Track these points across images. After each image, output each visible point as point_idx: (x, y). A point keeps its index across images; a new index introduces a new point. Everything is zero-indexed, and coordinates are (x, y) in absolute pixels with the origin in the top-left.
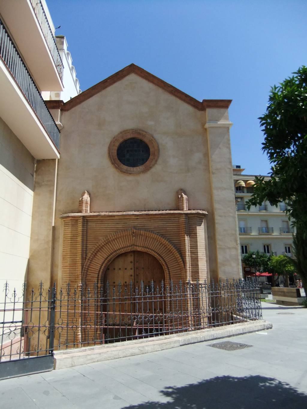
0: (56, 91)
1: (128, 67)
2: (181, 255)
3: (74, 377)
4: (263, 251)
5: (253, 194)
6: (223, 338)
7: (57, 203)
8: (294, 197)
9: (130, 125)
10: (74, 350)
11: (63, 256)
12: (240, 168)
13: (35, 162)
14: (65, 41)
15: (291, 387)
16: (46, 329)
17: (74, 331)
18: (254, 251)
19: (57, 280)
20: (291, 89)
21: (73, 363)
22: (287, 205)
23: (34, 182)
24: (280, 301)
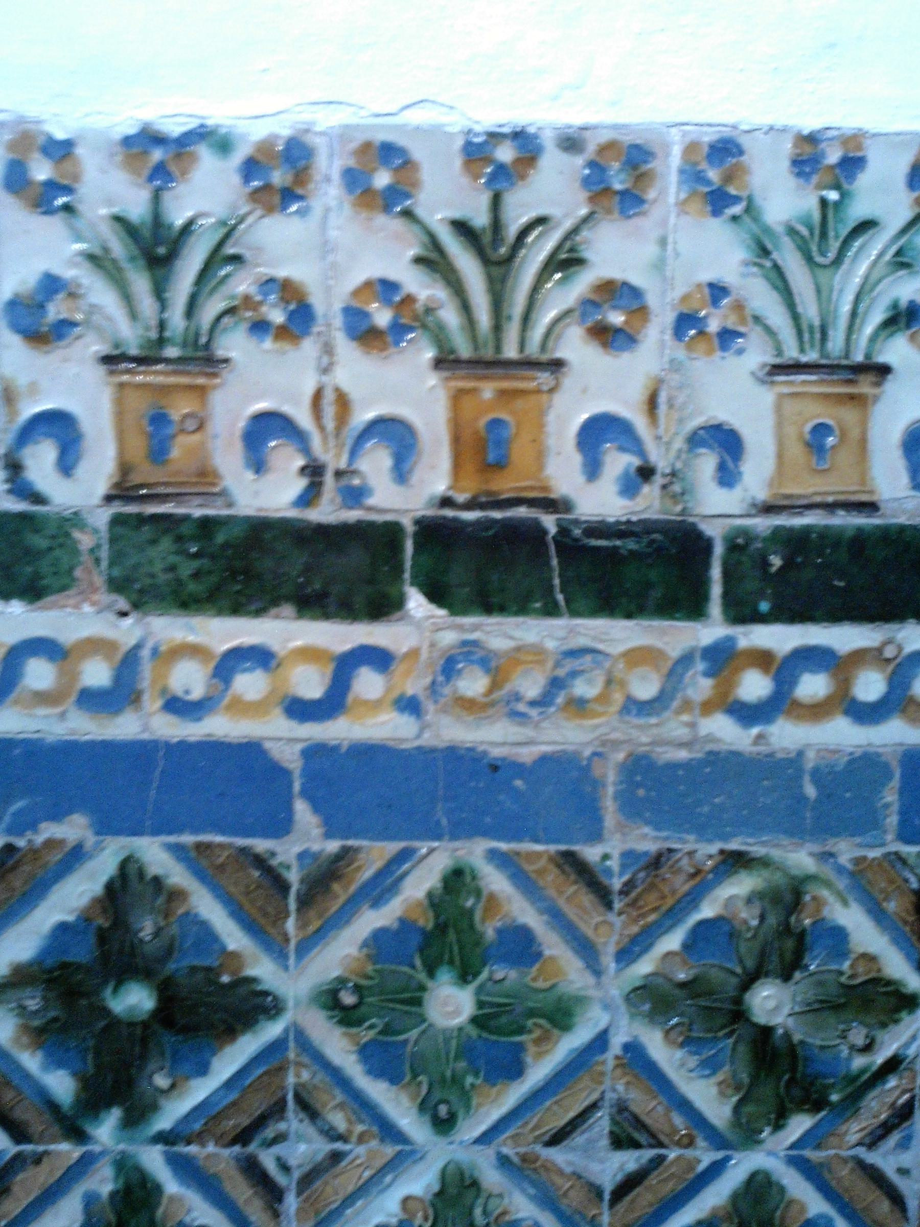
0: (401, 839)
2: (96, 550)
10: (811, 490)
13: (638, 172)
18: (206, 208)
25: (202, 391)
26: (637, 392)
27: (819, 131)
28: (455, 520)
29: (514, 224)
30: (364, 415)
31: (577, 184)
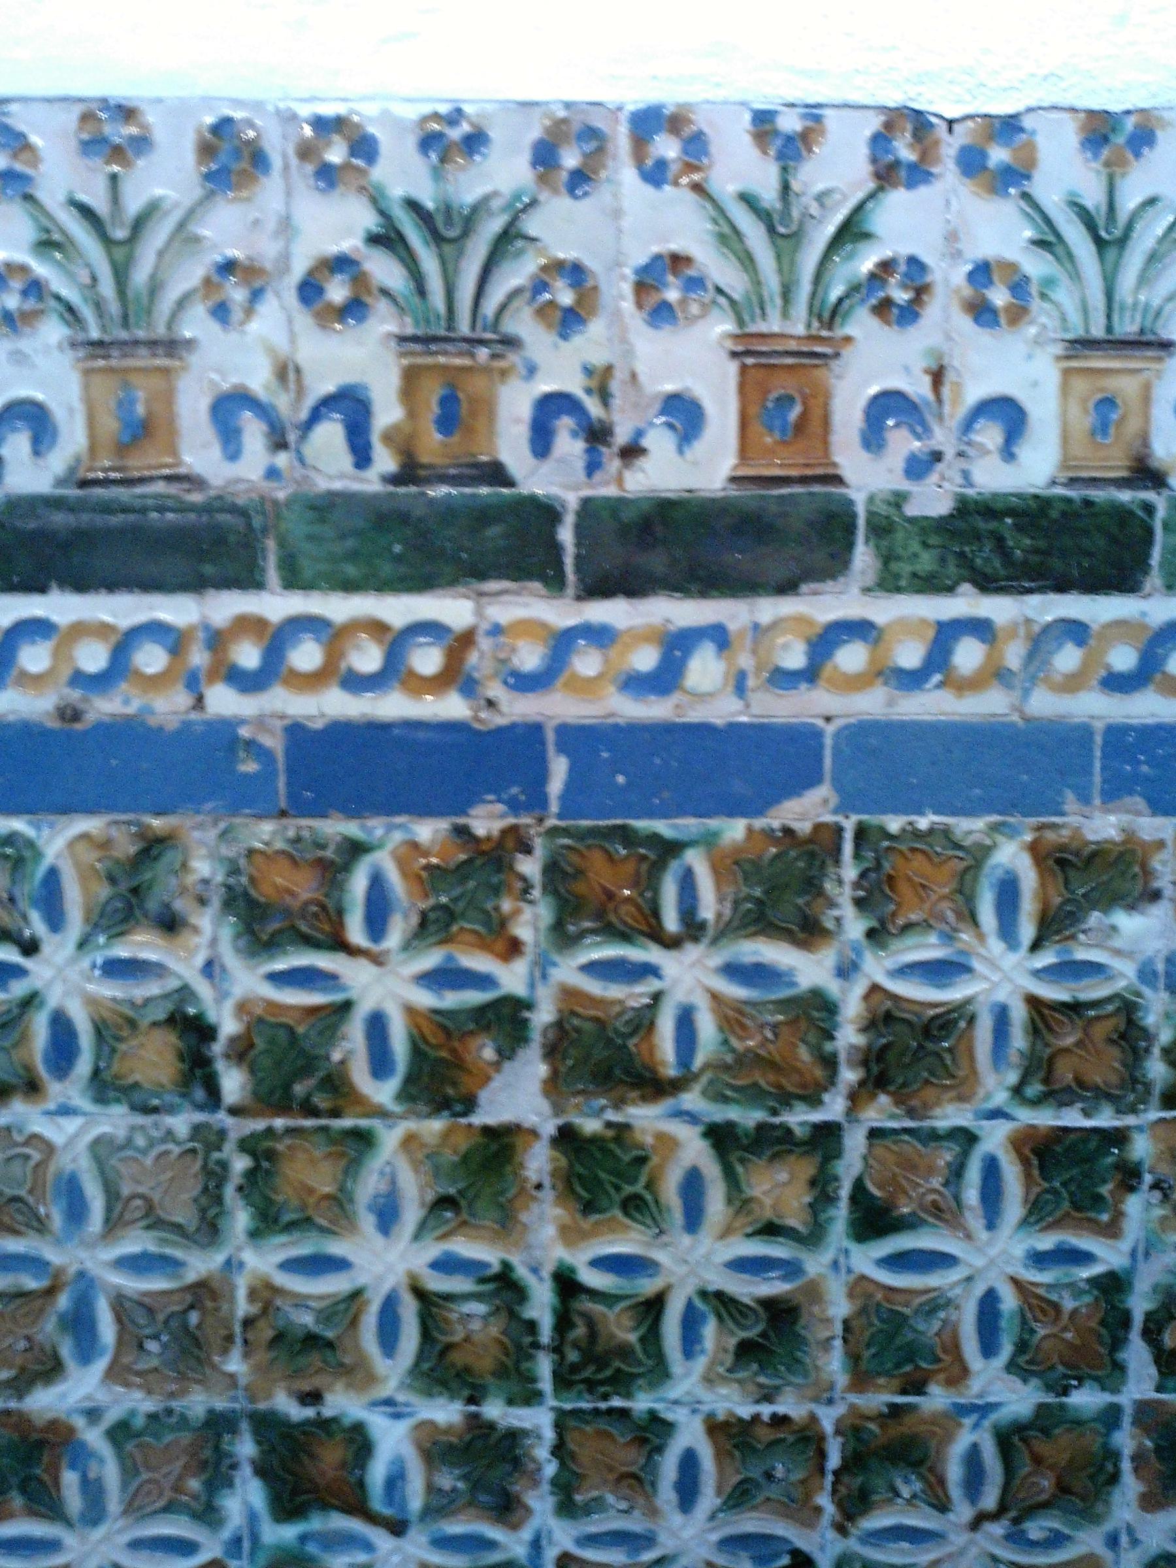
1: (647, 736)
5: (302, 1454)
11: (92, 1280)
13: (1075, 1049)
14: (1087, 987)
16: (221, 996)
20: (610, 1499)
21: (837, 196)
23: (402, 490)
24: (509, 101)
25: (166, 372)
26: (919, 364)
27: (697, 104)
28: (474, 495)
29: (133, 205)
30: (974, 393)
31: (1142, 160)
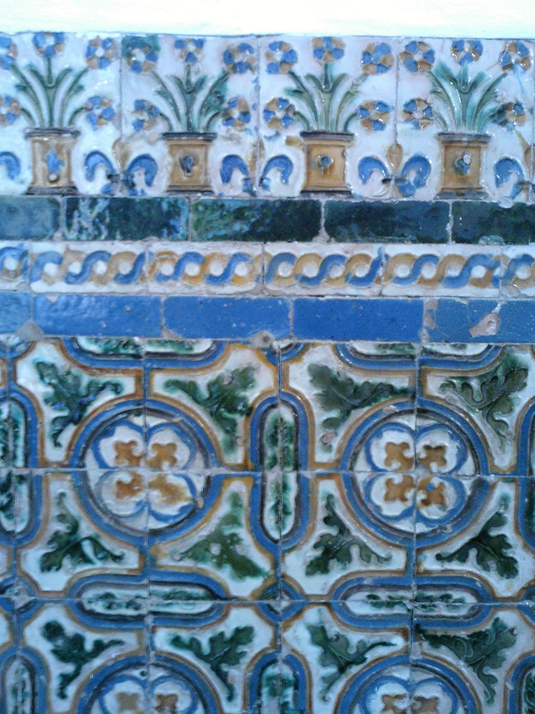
3: (407, 46)
4: (417, 682)
6: (102, 361)
7: (379, 38)
8: (232, 547)
9: (134, 100)
12: (269, 190)
14: (367, 413)
15: (128, 295)
17: (128, 129)
19: (91, 405)
22: (249, 169)
